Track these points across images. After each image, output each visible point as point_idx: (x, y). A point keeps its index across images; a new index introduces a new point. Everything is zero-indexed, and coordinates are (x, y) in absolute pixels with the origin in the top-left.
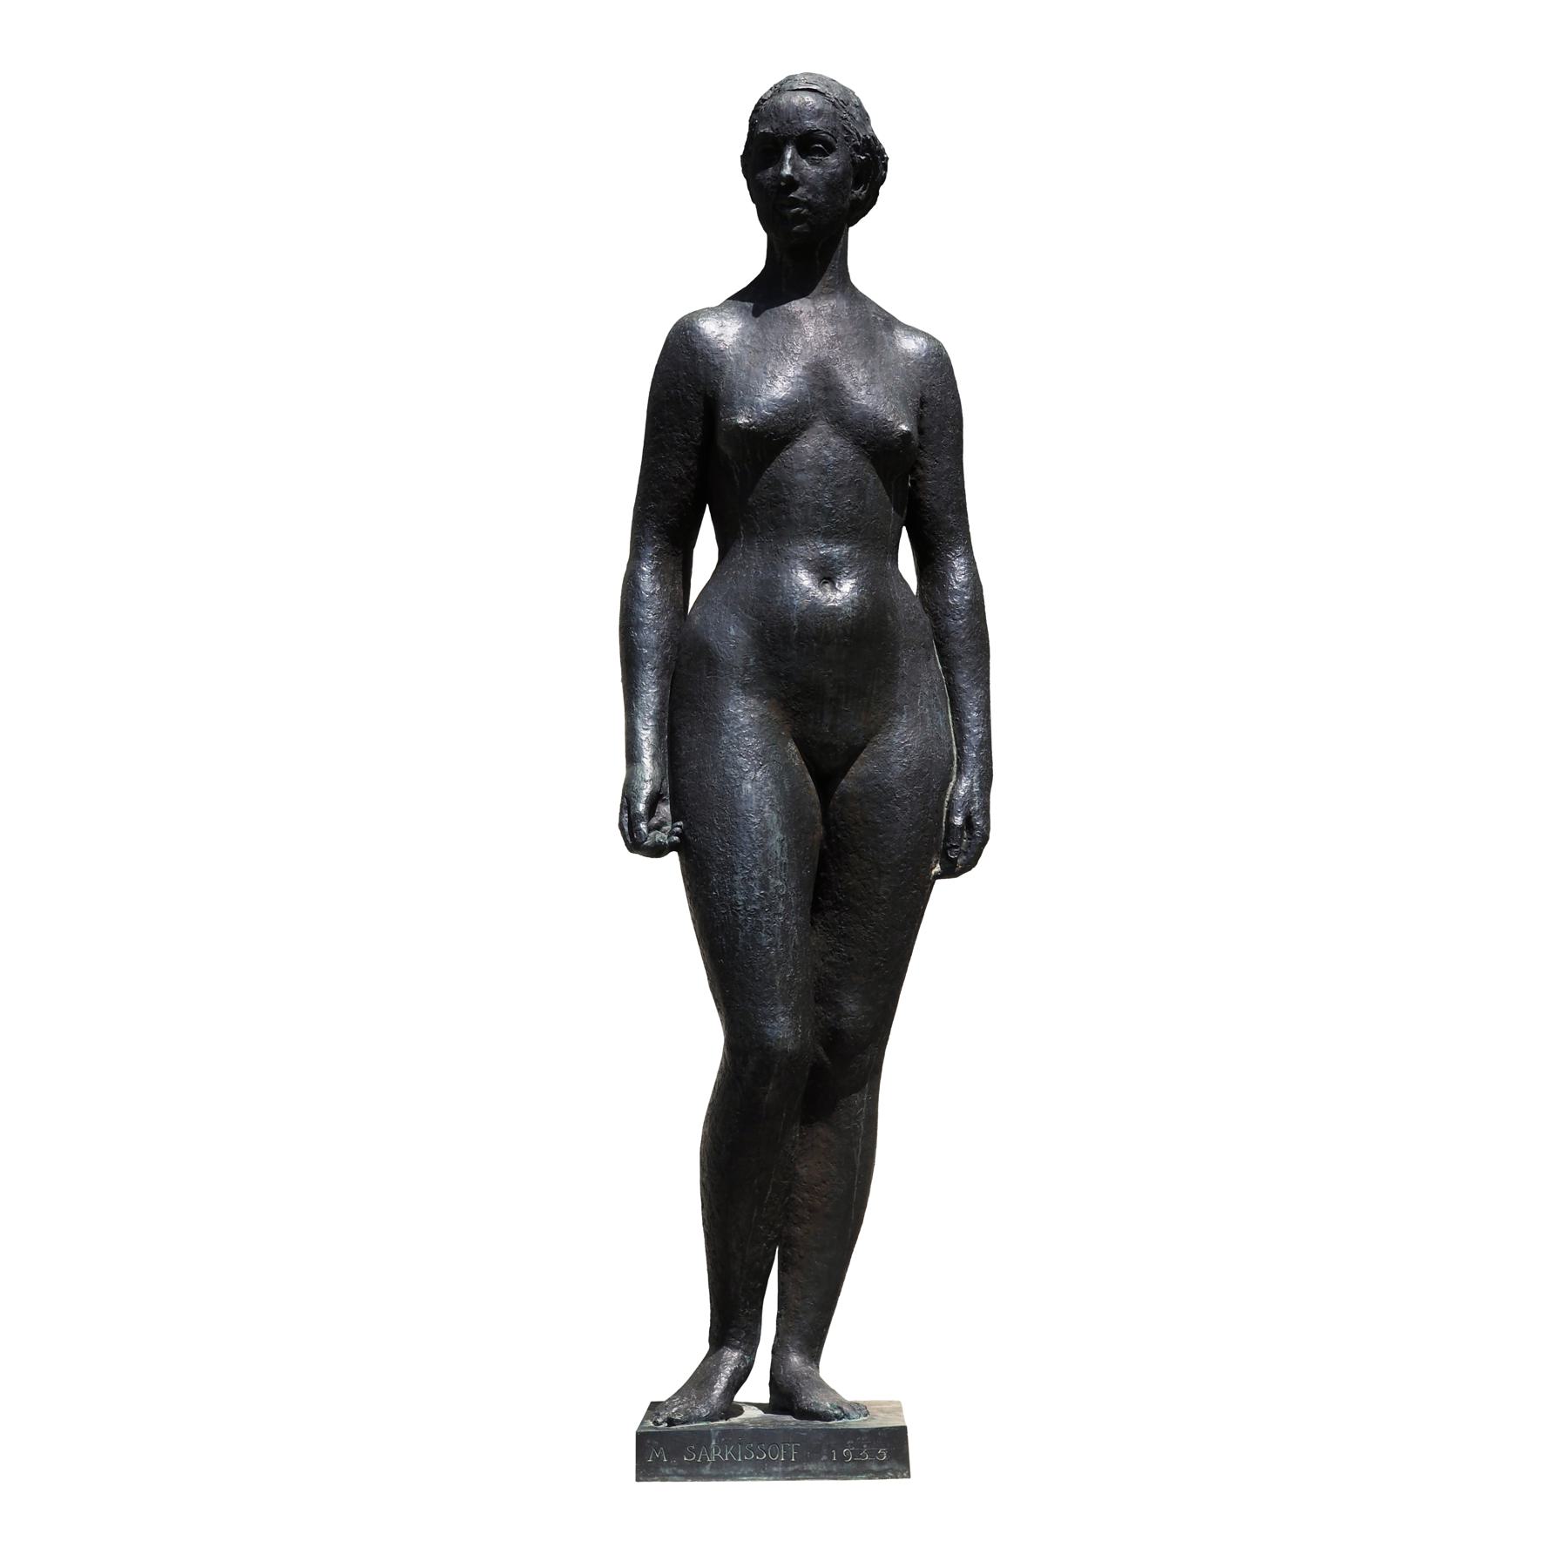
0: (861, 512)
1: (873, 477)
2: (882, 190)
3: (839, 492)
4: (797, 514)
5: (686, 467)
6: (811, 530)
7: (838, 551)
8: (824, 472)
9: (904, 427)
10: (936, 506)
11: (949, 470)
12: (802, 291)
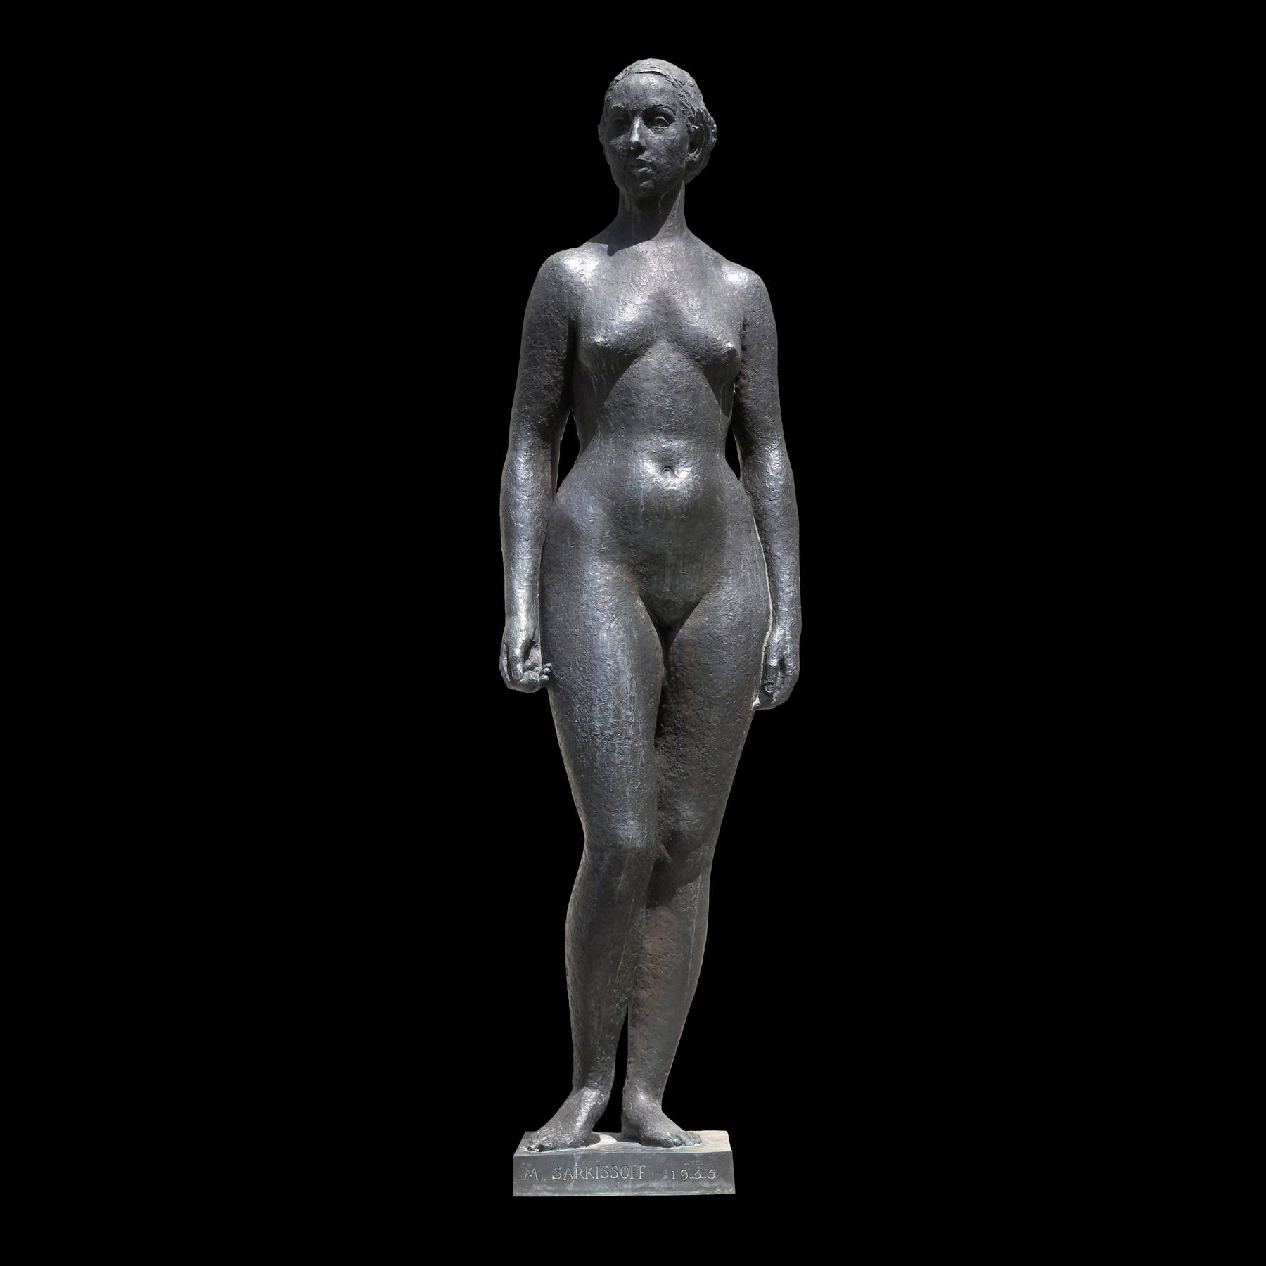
0: (696, 413)
3: (678, 398)
4: (643, 415)
5: (555, 377)
7: (677, 445)
8: (665, 381)
9: (730, 345)
10: (756, 409)
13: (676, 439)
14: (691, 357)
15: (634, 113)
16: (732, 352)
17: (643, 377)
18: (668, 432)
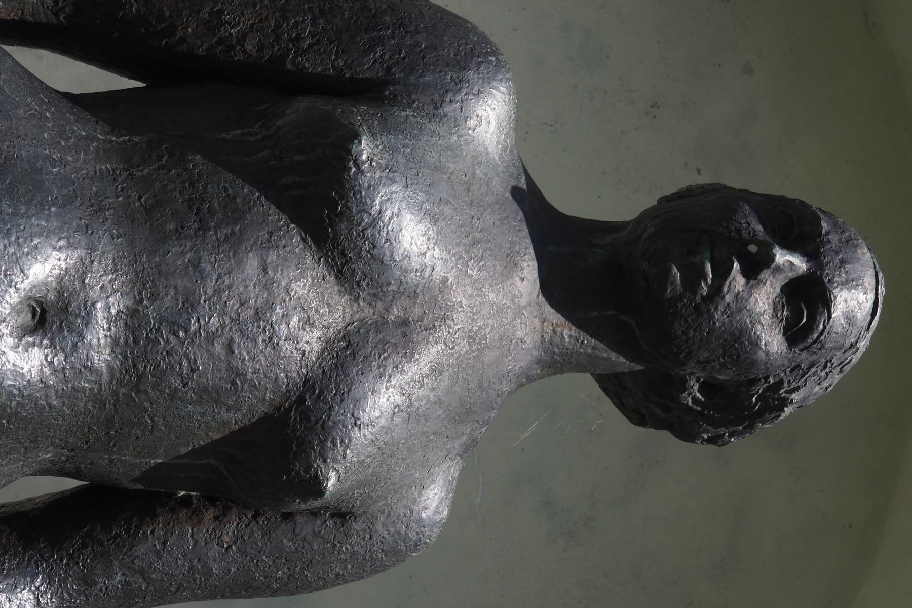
0: (173, 396)
1: (236, 419)
2: (666, 434)
3: (218, 348)
4: (178, 255)
5: (243, 37)
6: (144, 285)
7: (99, 341)
8: (258, 316)
9: (331, 483)
10: (141, 550)
11: (208, 573)
12: (553, 287)
13: (115, 342)
14: (308, 383)
15: (812, 255)
16: (316, 487)
17: (272, 257)
18: (132, 321)
